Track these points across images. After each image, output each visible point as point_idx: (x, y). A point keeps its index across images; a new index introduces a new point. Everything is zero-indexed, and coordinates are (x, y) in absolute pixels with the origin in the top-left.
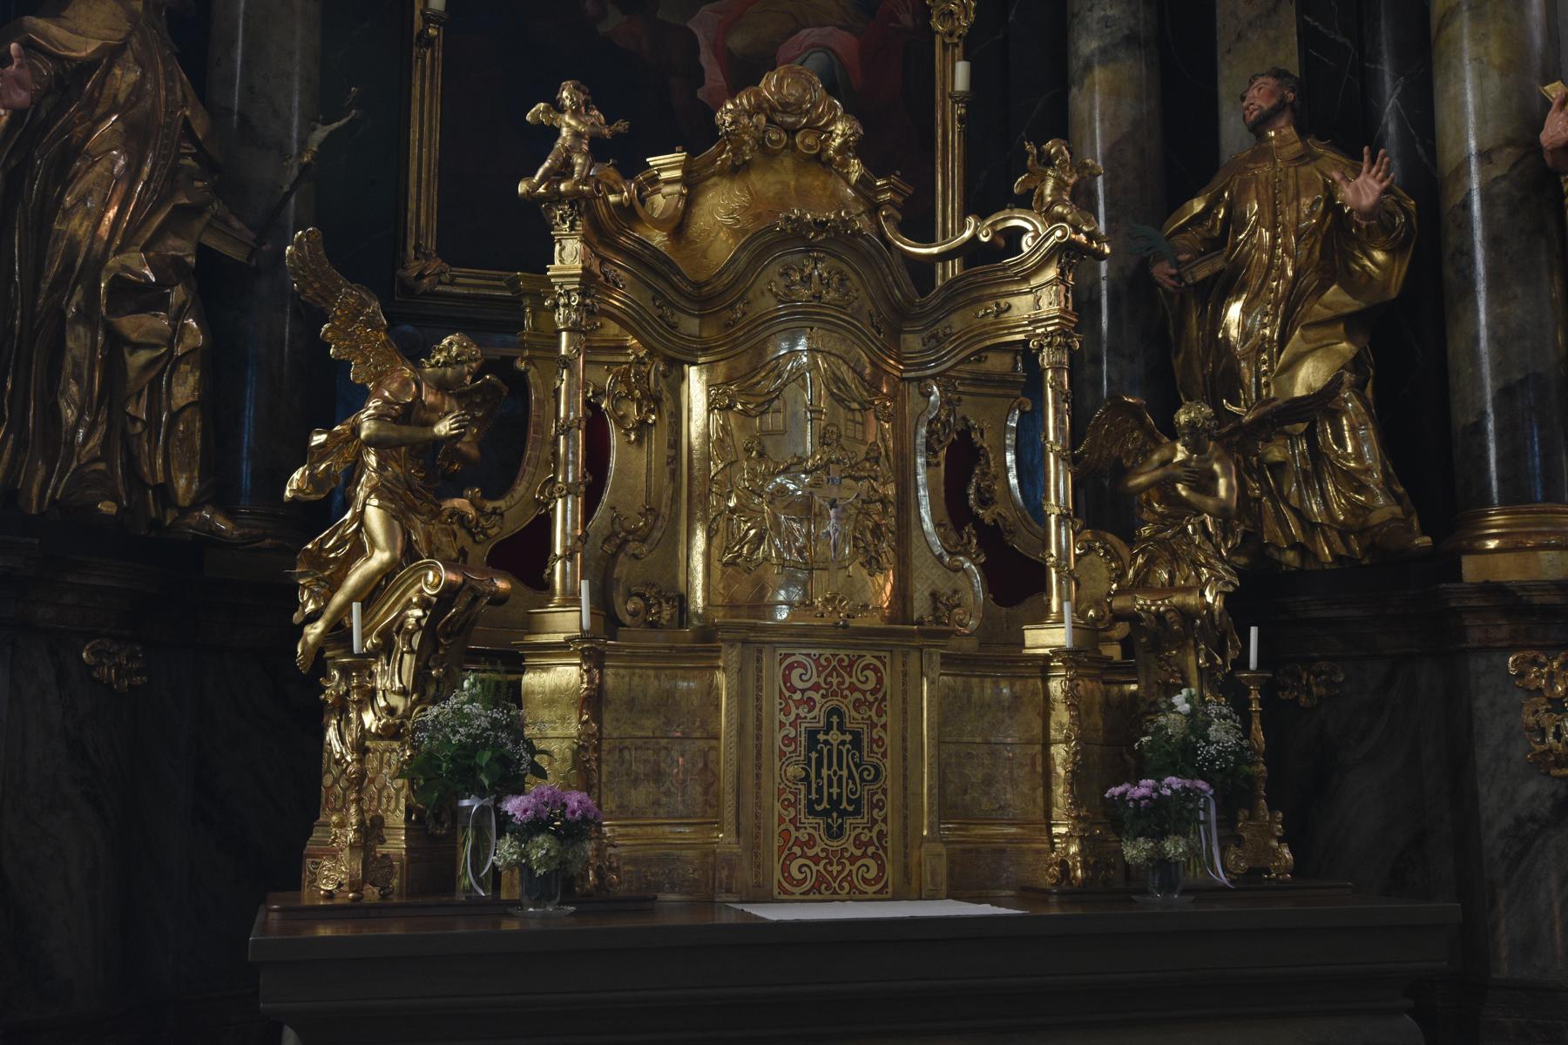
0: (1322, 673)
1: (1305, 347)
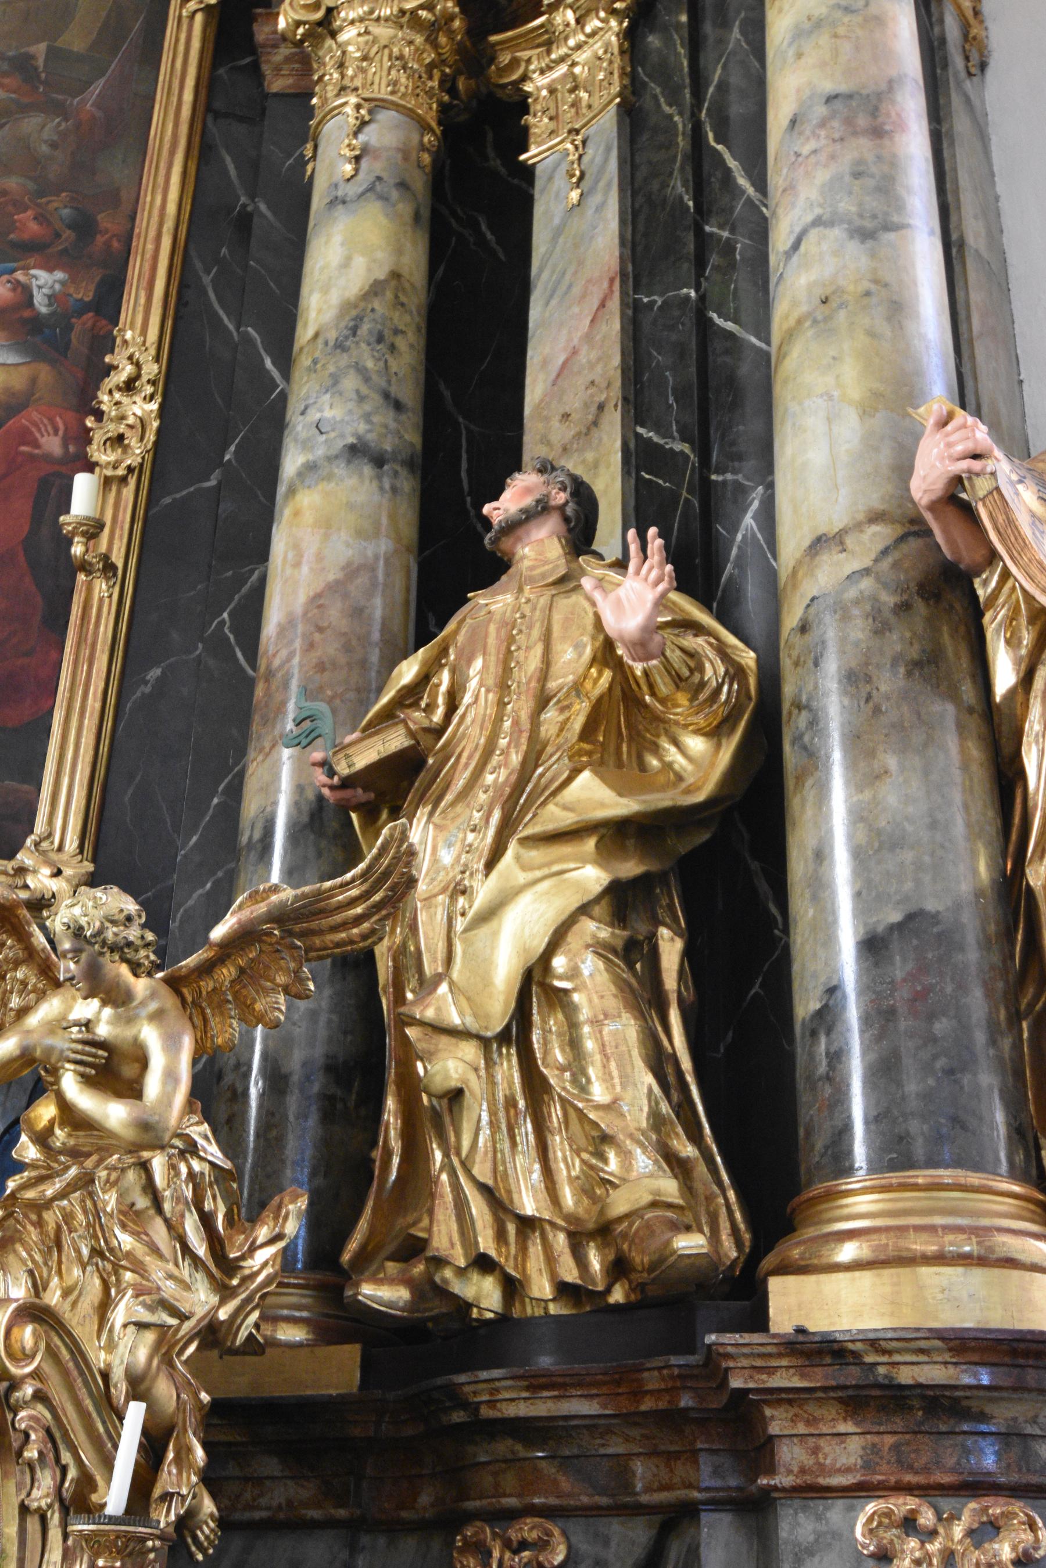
0: (523, 1545)
1: (522, 877)
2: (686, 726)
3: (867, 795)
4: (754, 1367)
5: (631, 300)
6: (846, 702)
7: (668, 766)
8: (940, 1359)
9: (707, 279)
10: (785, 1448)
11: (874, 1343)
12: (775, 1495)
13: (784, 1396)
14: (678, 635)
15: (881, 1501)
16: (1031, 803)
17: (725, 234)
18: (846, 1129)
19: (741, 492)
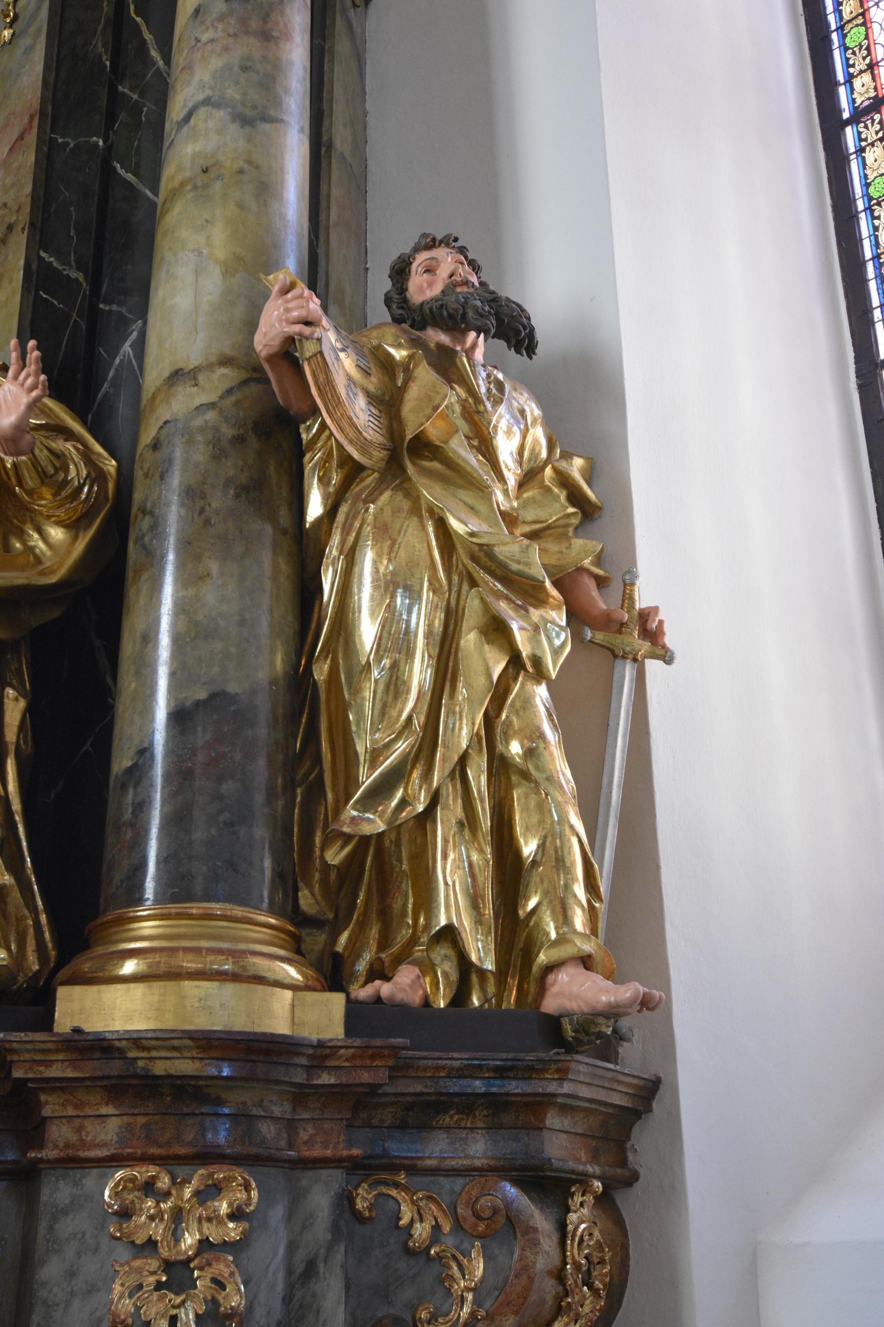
2: (49, 517)
3: (191, 592)
4: (34, 1061)
5: (47, 138)
6: (183, 513)
7: (31, 550)
8: (189, 1055)
9: (115, 132)
10: (54, 1128)
11: (137, 1040)
12: (41, 1166)
13: (58, 1084)
14: (48, 438)
15: (128, 1169)
16: (323, 613)
17: (135, 97)
18: (142, 865)
19: (123, 324)
